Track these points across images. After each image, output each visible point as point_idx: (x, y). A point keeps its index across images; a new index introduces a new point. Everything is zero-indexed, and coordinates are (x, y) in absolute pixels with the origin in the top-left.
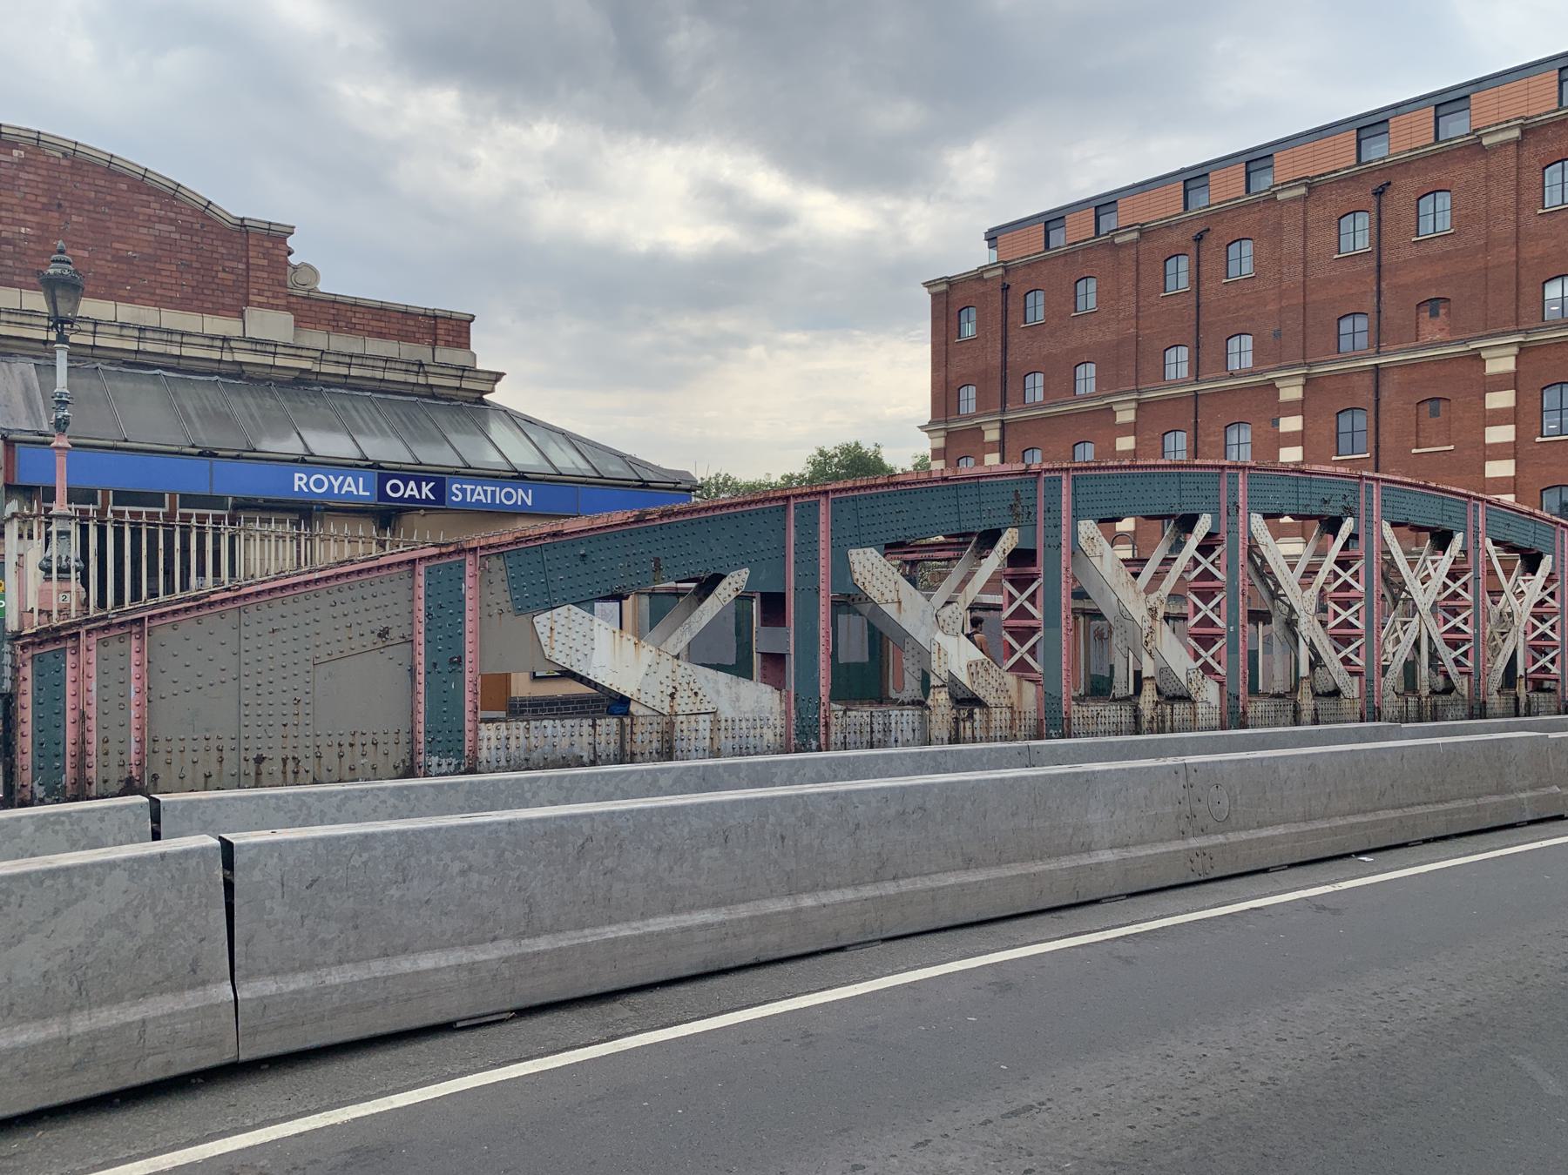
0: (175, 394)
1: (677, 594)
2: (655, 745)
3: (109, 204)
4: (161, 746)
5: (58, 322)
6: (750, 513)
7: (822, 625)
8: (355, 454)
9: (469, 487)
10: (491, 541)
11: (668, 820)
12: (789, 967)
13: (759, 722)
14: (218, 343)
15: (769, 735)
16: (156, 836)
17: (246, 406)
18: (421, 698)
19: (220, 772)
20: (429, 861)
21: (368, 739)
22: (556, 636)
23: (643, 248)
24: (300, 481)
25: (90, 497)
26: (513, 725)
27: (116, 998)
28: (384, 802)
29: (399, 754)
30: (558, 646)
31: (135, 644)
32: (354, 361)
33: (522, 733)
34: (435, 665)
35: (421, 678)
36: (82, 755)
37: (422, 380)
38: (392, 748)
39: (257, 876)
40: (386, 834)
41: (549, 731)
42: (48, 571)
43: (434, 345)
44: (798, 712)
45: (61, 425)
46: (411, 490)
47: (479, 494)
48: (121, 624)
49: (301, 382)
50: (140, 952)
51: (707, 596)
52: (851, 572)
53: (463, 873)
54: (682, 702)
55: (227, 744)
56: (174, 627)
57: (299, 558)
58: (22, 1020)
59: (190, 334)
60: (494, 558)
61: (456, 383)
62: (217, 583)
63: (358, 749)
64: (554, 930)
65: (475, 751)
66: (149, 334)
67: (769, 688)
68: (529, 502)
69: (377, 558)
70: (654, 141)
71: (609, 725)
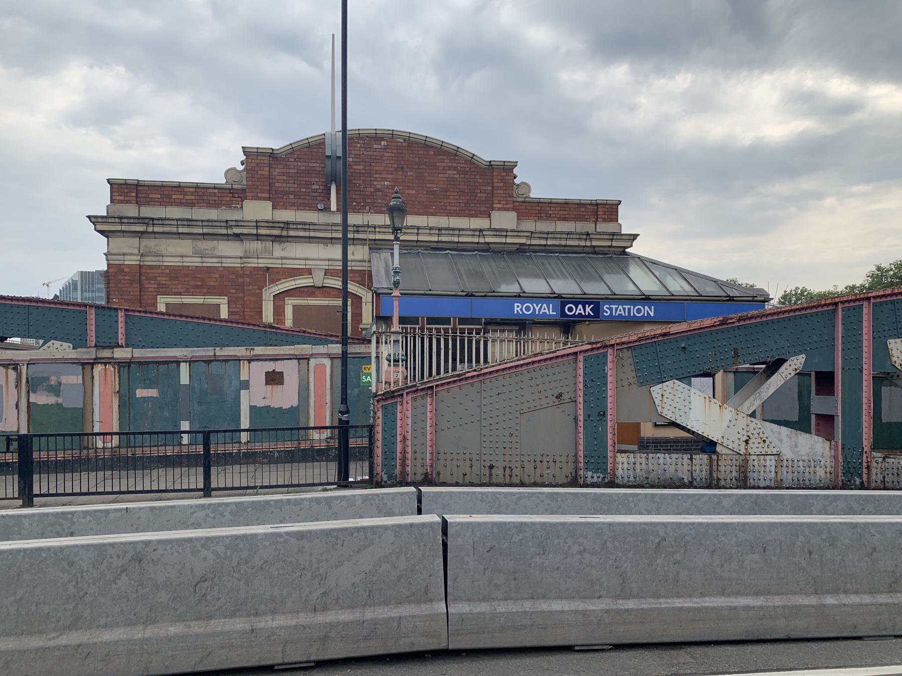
0: (456, 264)
1: (754, 372)
2: (734, 474)
3: (425, 164)
4: (442, 456)
5: (396, 230)
6: (806, 316)
7: (865, 395)
8: (548, 291)
9: (614, 307)
10: (624, 340)
11: (721, 533)
12: (814, 646)
13: (813, 462)
14: (477, 233)
15: (821, 473)
16: (419, 512)
17: (491, 268)
18: (581, 436)
19: (471, 473)
20: (559, 543)
21: (550, 459)
22: (665, 400)
23: (747, 142)
24: (518, 308)
25: (414, 321)
26: (638, 455)
27: (386, 603)
28: (543, 501)
29: (568, 469)
30: (667, 407)
31: (429, 400)
32: (550, 236)
33: (643, 461)
34: (589, 416)
35: (581, 424)
36: (404, 459)
37: (588, 244)
38: (564, 464)
39: (460, 541)
40: (533, 524)
41: (661, 461)
42: (390, 361)
43: (596, 222)
44: (845, 458)
45: (396, 284)
46: (580, 310)
47: (620, 310)
48: (423, 389)
49: (521, 251)
50: (399, 578)
51: (773, 374)
52: (889, 356)
53: (580, 552)
54: (754, 446)
55: (475, 457)
56: (472, 385)
57: (517, 351)
58: (342, 608)
59: (463, 230)
60: (625, 350)
61: (609, 243)
62: (470, 367)
63: (545, 464)
64: (639, 596)
65: (614, 470)
66: (443, 232)
67: (821, 439)
68: (652, 314)
69: (555, 352)
70: (756, 72)
71: (701, 459)
